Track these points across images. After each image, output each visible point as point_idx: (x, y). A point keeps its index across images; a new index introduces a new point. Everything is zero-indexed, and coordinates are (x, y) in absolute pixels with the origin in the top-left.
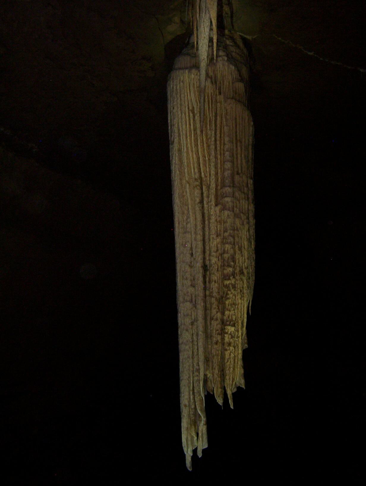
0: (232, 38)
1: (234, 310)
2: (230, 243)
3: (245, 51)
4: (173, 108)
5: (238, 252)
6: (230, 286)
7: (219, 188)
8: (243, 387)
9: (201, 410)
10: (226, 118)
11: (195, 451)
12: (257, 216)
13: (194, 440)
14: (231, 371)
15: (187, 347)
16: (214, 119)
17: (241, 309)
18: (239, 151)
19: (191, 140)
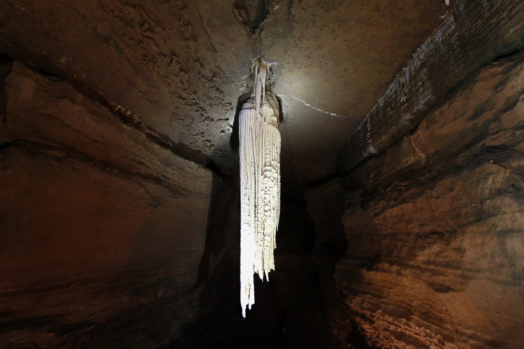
11: (247, 306)
13: (247, 298)
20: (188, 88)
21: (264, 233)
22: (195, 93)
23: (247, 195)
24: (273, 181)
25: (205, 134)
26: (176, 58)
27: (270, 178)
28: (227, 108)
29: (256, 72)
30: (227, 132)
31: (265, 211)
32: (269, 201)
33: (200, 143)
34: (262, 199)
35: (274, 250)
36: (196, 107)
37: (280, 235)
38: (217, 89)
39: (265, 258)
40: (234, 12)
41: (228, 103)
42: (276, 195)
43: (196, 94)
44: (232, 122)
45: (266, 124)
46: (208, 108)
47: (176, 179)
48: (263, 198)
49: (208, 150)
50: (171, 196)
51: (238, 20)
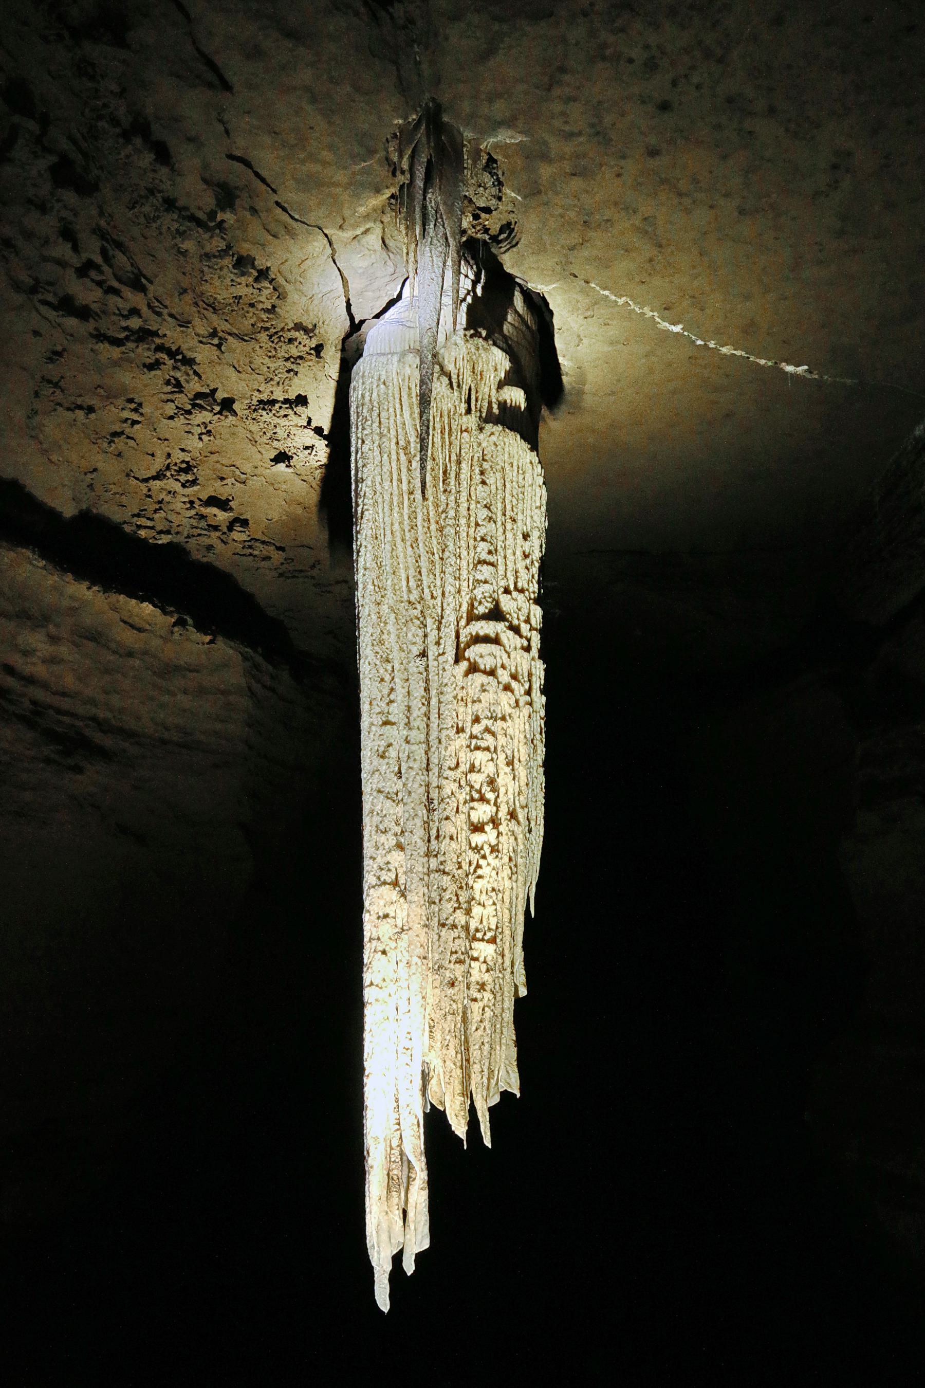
1: (494, 904)
3: (529, 318)
4: (363, 442)
6: (486, 847)
11: (397, 1259)
13: (396, 1224)
14: (485, 1053)
16: (454, 468)
17: (511, 903)
20: (99, 260)
21: (466, 928)
22: (137, 283)
23: (392, 753)
24: (507, 688)
25: (202, 473)
26: (32, 125)
27: (492, 673)
28: (294, 352)
29: (420, 183)
30: (301, 459)
31: (477, 828)
32: (492, 782)
33: (180, 516)
34: (457, 774)
36: (144, 353)
37: (545, 935)
38: (243, 263)
39: (476, 1037)
41: (298, 327)
42: (523, 752)
43: (143, 289)
44: (322, 412)
46: (203, 354)
47: (69, 681)
48: (463, 768)
49: (219, 546)
50: (48, 761)
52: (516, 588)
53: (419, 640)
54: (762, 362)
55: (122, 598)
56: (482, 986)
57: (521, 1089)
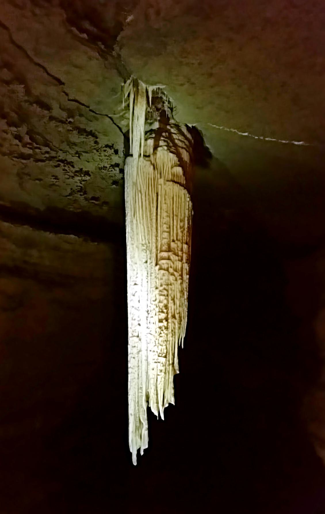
0: (177, 126)
2: (164, 295)
5: (171, 301)
7: (159, 252)
8: (173, 403)
9: (143, 419)
10: (165, 197)
11: (139, 451)
12: (191, 273)
13: (138, 440)
15: (134, 371)
18: (175, 223)
19: (139, 214)
24: (172, 274)
35: (176, 377)
40: (70, 31)
41: (107, 146)
45: (161, 181)
51: (82, 41)
52: (177, 239)
53: (145, 257)
54: (284, 142)
55: (62, 235)
56: (161, 371)
57: (175, 403)
